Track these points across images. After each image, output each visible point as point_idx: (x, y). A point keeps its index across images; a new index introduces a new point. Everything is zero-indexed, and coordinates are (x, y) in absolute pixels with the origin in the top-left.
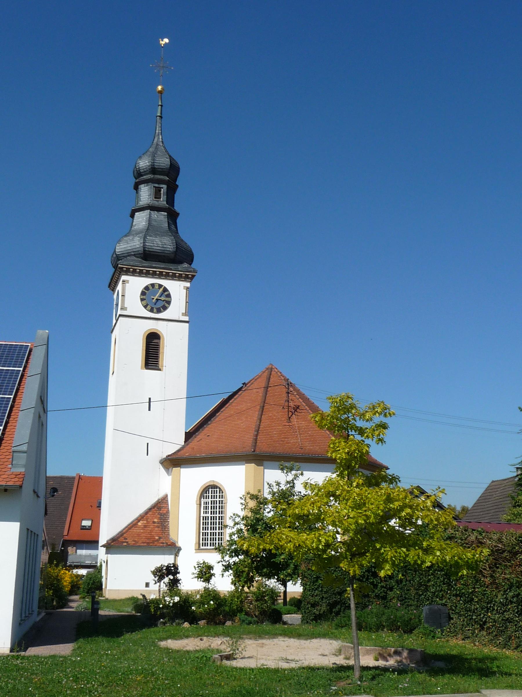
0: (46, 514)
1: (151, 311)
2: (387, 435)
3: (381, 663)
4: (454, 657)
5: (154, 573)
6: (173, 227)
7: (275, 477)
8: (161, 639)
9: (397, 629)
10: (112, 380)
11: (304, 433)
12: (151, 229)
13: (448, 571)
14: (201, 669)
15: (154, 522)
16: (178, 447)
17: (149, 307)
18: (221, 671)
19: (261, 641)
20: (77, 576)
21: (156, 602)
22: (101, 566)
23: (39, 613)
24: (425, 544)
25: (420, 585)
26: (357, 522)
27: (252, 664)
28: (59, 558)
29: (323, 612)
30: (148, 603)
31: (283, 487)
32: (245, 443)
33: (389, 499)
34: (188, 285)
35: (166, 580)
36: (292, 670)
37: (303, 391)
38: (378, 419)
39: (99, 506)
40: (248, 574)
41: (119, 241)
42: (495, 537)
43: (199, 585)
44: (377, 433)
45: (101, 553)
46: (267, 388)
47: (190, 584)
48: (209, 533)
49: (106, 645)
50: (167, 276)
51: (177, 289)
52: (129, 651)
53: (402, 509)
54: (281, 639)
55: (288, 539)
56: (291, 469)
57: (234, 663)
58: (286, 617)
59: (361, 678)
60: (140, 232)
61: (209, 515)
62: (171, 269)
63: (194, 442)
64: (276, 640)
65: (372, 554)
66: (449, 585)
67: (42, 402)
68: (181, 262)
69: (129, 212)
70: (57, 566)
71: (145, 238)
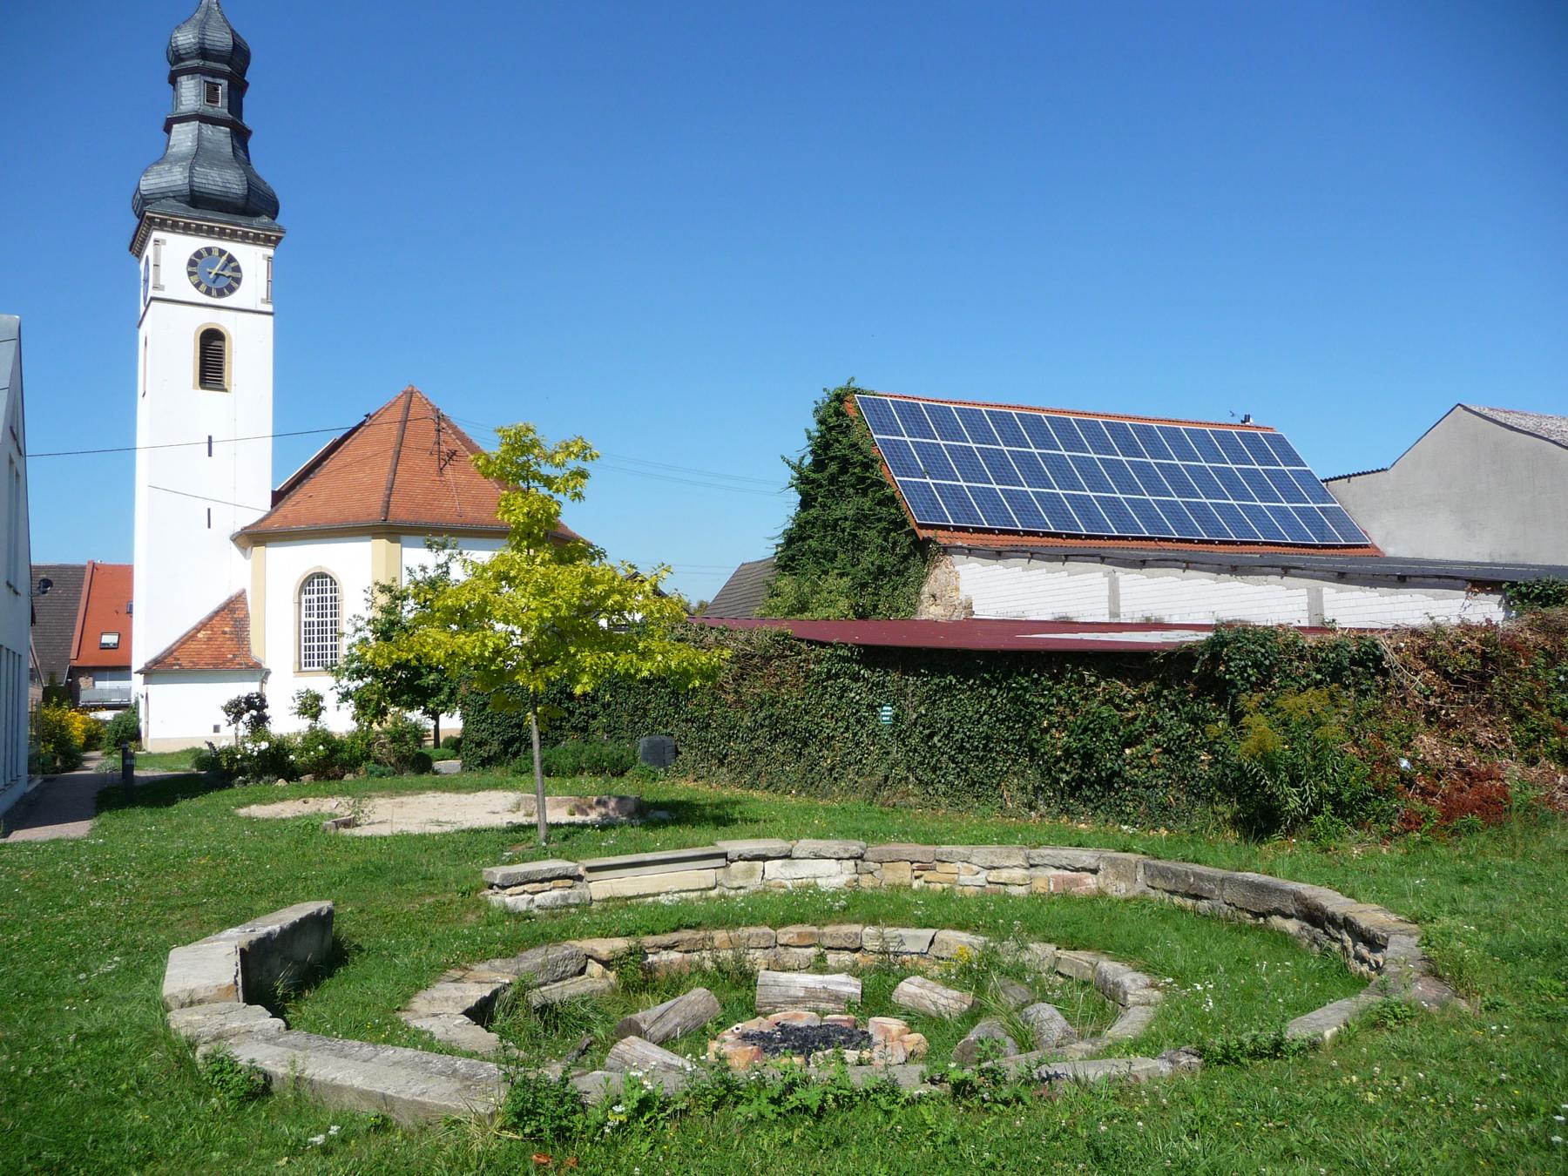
0: (33, 621)
1: (208, 292)
2: (587, 487)
3: (578, 818)
4: (680, 804)
5: (227, 710)
6: (241, 153)
7: (419, 559)
8: (240, 806)
9: (603, 771)
10: (143, 408)
11: (465, 492)
12: (200, 154)
13: (671, 685)
14: (304, 842)
15: (224, 633)
16: (261, 515)
17: (203, 287)
18: (333, 843)
19: (399, 799)
20: (97, 721)
21: (230, 752)
22: (137, 703)
23: (30, 781)
24: (641, 646)
25: (636, 708)
26: (540, 616)
27: (385, 831)
28: (64, 693)
29: (494, 753)
30: (217, 754)
31: (431, 573)
32: (370, 507)
33: (589, 582)
34: (270, 252)
35: (246, 717)
36: (445, 835)
37: (462, 428)
38: (573, 464)
39: (130, 612)
40: (378, 703)
41: (146, 171)
42: (742, 637)
43: (303, 724)
44: (572, 484)
45: (136, 685)
46: (405, 422)
47: (285, 723)
48: (316, 646)
49: (148, 819)
50: (233, 236)
51: (252, 259)
52: (188, 825)
53: (608, 595)
54: (430, 794)
55: (437, 642)
56: (444, 547)
57: (357, 832)
58: (437, 765)
59: (547, 839)
60: (183, 159)
61: (315, 619)
63: (287, 507)
64: (422, 797)
65: (564, 662)
66: (677, 706)
67: (15, 437)
68: (257, 214)
69: (162, 123)
70: (59, 705)
71: (192, 168)
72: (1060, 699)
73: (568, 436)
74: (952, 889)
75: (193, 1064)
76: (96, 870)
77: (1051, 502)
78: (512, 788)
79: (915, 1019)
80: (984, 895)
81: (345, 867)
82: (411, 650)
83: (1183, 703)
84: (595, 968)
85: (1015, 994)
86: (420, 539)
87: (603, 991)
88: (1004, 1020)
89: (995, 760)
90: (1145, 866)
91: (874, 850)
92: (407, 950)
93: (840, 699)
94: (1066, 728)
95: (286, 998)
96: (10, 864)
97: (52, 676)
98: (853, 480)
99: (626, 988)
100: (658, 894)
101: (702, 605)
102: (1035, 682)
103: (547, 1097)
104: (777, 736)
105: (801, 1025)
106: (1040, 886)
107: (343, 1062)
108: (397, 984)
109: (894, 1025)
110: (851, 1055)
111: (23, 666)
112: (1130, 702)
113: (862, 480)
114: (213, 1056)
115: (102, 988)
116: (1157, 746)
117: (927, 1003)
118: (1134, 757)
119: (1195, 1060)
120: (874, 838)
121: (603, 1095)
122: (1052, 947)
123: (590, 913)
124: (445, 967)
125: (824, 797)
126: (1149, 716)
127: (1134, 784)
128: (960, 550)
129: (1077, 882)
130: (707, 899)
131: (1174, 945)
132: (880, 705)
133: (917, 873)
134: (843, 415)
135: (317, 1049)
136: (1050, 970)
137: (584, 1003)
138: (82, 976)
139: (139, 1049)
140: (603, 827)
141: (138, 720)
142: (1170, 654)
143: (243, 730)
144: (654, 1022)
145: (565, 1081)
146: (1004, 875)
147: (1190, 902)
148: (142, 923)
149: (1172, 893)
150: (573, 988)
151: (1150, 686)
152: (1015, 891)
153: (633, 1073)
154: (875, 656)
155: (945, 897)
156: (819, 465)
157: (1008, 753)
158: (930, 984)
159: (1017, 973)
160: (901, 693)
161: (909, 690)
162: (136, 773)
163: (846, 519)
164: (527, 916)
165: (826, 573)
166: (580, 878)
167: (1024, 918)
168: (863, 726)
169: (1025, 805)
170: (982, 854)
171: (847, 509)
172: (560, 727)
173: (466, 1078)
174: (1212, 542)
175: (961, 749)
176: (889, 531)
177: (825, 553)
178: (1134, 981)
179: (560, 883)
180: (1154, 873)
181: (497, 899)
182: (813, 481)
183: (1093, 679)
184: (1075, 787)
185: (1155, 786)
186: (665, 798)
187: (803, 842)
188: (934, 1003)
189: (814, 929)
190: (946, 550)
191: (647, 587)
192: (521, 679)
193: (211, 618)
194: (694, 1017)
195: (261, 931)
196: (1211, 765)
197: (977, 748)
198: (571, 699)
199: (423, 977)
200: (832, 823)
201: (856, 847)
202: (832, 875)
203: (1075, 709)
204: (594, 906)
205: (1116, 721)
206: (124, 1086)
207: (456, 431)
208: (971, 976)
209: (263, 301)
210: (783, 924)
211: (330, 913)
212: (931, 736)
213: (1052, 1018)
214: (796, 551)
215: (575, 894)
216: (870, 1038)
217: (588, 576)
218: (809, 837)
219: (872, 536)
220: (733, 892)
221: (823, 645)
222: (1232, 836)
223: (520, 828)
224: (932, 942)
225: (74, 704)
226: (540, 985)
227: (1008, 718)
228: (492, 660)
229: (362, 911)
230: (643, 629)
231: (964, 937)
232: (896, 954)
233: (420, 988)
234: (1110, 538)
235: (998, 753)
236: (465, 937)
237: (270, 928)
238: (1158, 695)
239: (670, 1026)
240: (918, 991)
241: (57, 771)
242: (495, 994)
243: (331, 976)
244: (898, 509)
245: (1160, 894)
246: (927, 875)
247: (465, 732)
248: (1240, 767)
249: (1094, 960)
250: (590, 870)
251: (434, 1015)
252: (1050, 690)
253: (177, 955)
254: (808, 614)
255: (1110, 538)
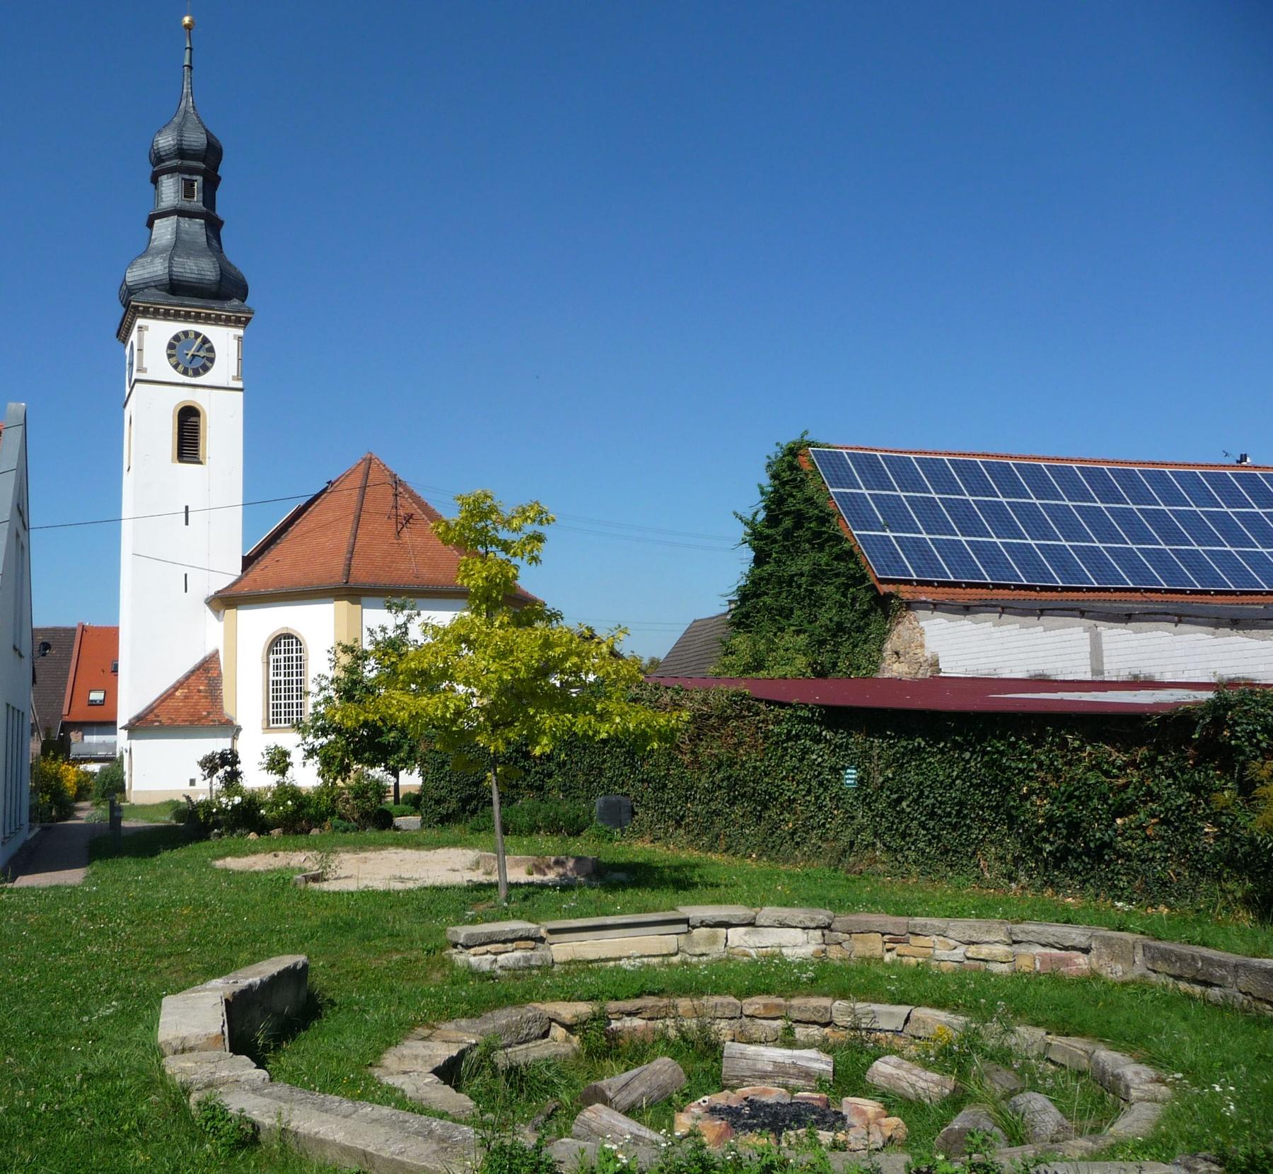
0: (34, 681)
1: (185, 372)
2: (544, 550)
3: (537, 878)
4: (639, 865)
5: (203, 764)
6: (214, 243)
9: (559, 831)
10: (128, 480)
11: (421, 555)
12: (179, 245)
13: (631, 747)
15: (199, 691)
16: (232, 579)
17: (181, 368)
18: (304, 896)
19: (363, 855)
20: (86, 773)
21: (207, 805)
22: (122, 757)
23: (30, 829)
24: (599, 707)
25: (591, 767)
26: (500, 678)
27: (351, 886)
28: (58, 747)
32: (333, 571)
33: (547, 644)
34: (240, 332)
35: (221, 772)
36: (409, 891)
37: (418, 492)
38: (530, 528)
39: (115, 671)
41: (131, 265)
42: (698, 697)
43: (271, 780)
44: (529, 548)
45: (121, 739)
46: (364, 488)
48: (283, 702)
49: (135, 869)
50: (207, 319)
51: (224, 339)
52: (170, 875)
53: (565, 657)
54: (392, 850)
55: (400, 704)
56: (403, 608)
57: (325, 886)
58: (398, 821)
59: (508, 899)
61: (282, 678)
64: (384, 853)
65: (523, 723)
66: (632, 766)
67: (21, 513)
69: (145, 220)
70: (55, 758)
71: (171, 258)
72: (1041, 764)
73: (525, 502)
74: (927, 964)
75: (186, 1109)
76: (92, 917)
77: (1023, 554)
78: (471, 846)
79: (892, 1101)
80: (962, 971)
81: (316, 921)
82: (376, 712)
83: (1183, 770)
84: (558, 1032)
85: (1001, 1080)
86: (381, 600)
87: (567, 1055)
88: (990, 1109)
89: (970, 828)
90: (1144, 946)
91: (842, 920)
92: (377, 1006)
93: (801, 760)
94: (1048, 795)
95: (266, 1048)
96: (17, 907)
97: (48, 731)
98: (809, 534)
99: (589, 1054)
100: (620, 959)
101: (654, 663)
102: (1013, 746)
103: (523, 1164)
104: (735, 798)
105: (771, 1101)
106: (1025, 964)
107: (325, 1116)
108: (368, 1039)
109: (870, 1106)
110: (825, 1136)
111: (26, 720)
112: (1119, 768)
113: (818, 534)
114: (206, 1104)
115: (102, 1031)
116: (1154, 816)
117: (905, 1084)
118: (1126, 828)
119: (1215, 1168)
120: (841, 907)
121: (578, 1166)
122: (1041, 1032)
123: (552, 975)
124: (413, 1025)
125: (786, 861)
126: (1142, 784)
127: (1128, 857)
128: (924, 605)
129: (1067, 962)
130: (669, 965)
131: (1183, 1036)
132: (844, 768)
133: (889, 946)
134: (797, 469)
135: (300, 1102)
136: (1040, 1057)
137: (548, 1067)
138: (86, 1019)
139: (138, 1091)
140: (564, 888)
141: (123, 773)
142: (1165, 718)
143: (217, 784)
144: (620, 1090)
145: (538, 1148)
146: (984, 951)
147: (1198, 989)
148: (135, 969)
149: (1178, 978)
150: (536, 1051)
151: (1143, 751)
152: (997, 968)
153: (607, 1146)
154: (837, 717)
155: (920, 973)
156: (772, 520)
157: (984, 820)
158: (907, 1065)
159: (1003, 1057)
160: (866, 755)
161: (875, 752)
162: (124, 824)
163: (802, 575)
164: (489, 977)
165: (782, 630)
166: (542, 940)
167: (1009, 998)
168: (826, 789)
169: (1004, 876)
170: (960, 928)
171: (803, 564)
172: (516, 786)
173: (442, 1140)
174: (1207, 593)
175: (932, 815)
176: (847, 586)
177: (781, 611)
178: (1137, 1073)
179: (522, 944)
180: (1155, 956)
181: (463, 958)
182: (767, 537)
183: (1077, 743)
184: (1060, 858)
185: (1153, 859)
186: (622, 860)
187: (767, 910)
188: (913, 1086)
189: (781, 1001)
190: (910, 606)
191: (604, 649)
192: (481, 740)
193: (187, 677)
194: (660, 1087)
195: (244, 983)
196: (1216, 838)
197: (949, 815)
198: (524, 758)
199: (392, 1033)
200: (795, 889)
201: (823, 916)
202: (798, 944)
203: (1057, 774)
204: (556, 969)
205: (1104, 788)
206: (126, 1127)
207: (412, 495)
208: (950, 1058)
210: (749, 993)
211: (305, 966)
212: (899, 801)
213: (1044, 1110)
214: (750, 608)
215: (538, 955)
216: (844, 1119)
217: (546, 639)
218: (772, 904)
219: (829, 591)
220: (695, 959)
221: (782, 705)
222: (1246, 919)
223: (480, 887)
224: (907, 1020)
225: (67, 759)
226: (504, 1047)
227: (983, 783)
228: (454, 721)
229: (333, 966)
230: (598, 690)
231: (943, 1016)
232: (869, 1031)
233: (389, 1045)
234: (1089, 590)
235: (973, 820)
236: (431, 996)
237: (250, 980)
238: (1152, 762)
239: (634, 1096)
240: (894, 1071)
241: (53, 820)
242: (462, 1054)
243: (306, 1028)
244: (857, 563)
245: (1162, 979)
246: (900, 948)
247: (424, 788)
248: (1252, 841)
249: (1090, 1048)
250: (552, 932)
251: (405, 1073)
252: (1029, 754)
253: (169, 1002)
254: (764, 673)
255: (1089, 590)
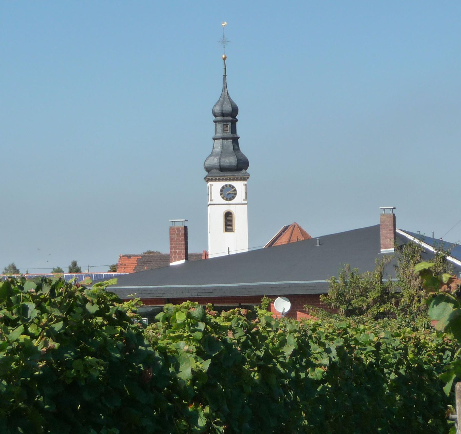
1: (226, 200)
17: (225, 198)
50: (233, 180)
51: (239, 186)
62: (235, 176)
71: (220, 159)
201: (380, 374)
209: (244, 200)
